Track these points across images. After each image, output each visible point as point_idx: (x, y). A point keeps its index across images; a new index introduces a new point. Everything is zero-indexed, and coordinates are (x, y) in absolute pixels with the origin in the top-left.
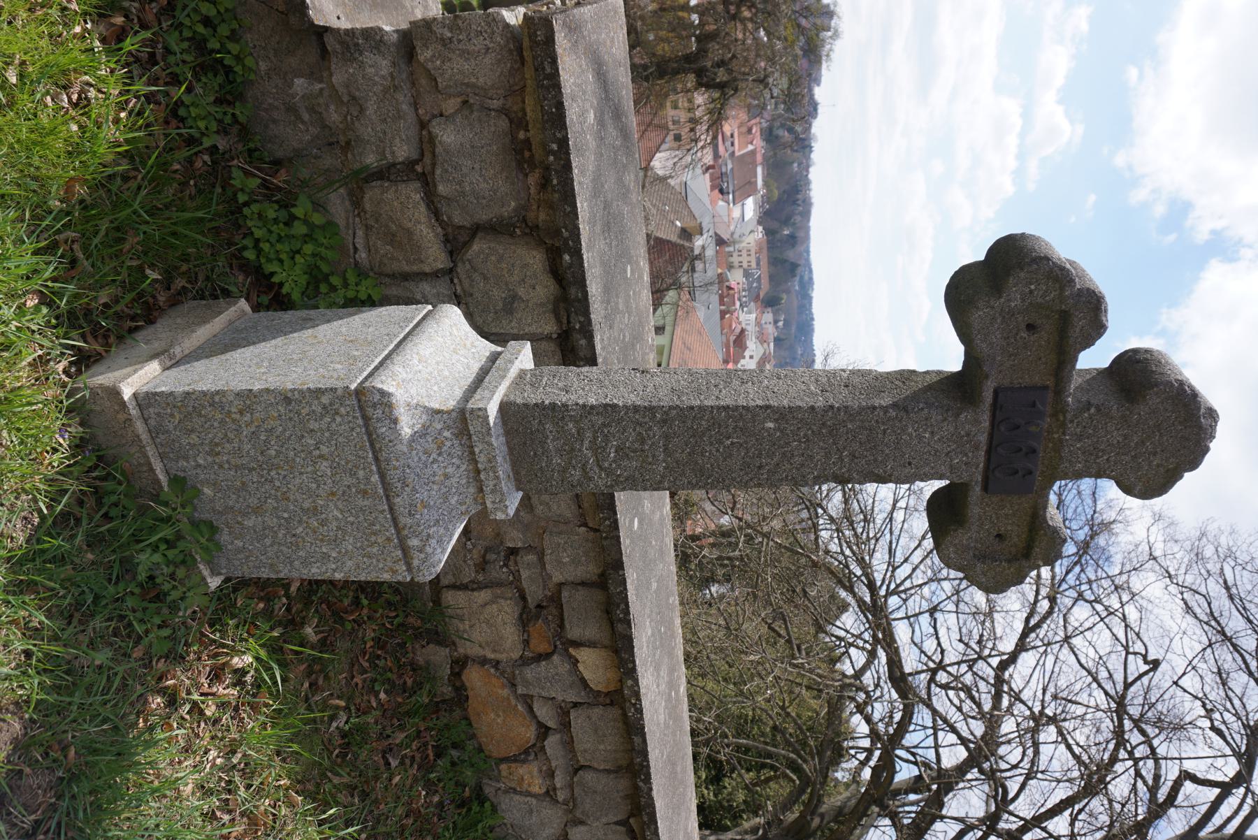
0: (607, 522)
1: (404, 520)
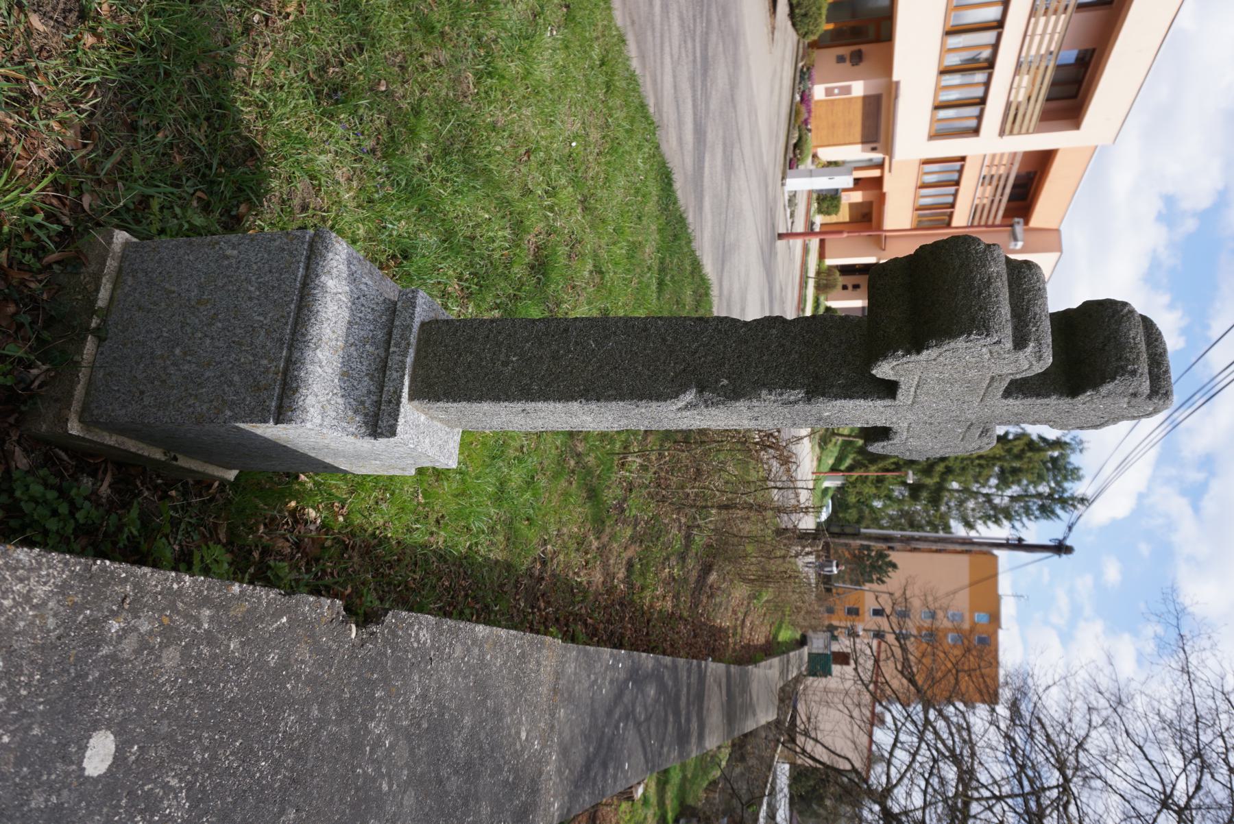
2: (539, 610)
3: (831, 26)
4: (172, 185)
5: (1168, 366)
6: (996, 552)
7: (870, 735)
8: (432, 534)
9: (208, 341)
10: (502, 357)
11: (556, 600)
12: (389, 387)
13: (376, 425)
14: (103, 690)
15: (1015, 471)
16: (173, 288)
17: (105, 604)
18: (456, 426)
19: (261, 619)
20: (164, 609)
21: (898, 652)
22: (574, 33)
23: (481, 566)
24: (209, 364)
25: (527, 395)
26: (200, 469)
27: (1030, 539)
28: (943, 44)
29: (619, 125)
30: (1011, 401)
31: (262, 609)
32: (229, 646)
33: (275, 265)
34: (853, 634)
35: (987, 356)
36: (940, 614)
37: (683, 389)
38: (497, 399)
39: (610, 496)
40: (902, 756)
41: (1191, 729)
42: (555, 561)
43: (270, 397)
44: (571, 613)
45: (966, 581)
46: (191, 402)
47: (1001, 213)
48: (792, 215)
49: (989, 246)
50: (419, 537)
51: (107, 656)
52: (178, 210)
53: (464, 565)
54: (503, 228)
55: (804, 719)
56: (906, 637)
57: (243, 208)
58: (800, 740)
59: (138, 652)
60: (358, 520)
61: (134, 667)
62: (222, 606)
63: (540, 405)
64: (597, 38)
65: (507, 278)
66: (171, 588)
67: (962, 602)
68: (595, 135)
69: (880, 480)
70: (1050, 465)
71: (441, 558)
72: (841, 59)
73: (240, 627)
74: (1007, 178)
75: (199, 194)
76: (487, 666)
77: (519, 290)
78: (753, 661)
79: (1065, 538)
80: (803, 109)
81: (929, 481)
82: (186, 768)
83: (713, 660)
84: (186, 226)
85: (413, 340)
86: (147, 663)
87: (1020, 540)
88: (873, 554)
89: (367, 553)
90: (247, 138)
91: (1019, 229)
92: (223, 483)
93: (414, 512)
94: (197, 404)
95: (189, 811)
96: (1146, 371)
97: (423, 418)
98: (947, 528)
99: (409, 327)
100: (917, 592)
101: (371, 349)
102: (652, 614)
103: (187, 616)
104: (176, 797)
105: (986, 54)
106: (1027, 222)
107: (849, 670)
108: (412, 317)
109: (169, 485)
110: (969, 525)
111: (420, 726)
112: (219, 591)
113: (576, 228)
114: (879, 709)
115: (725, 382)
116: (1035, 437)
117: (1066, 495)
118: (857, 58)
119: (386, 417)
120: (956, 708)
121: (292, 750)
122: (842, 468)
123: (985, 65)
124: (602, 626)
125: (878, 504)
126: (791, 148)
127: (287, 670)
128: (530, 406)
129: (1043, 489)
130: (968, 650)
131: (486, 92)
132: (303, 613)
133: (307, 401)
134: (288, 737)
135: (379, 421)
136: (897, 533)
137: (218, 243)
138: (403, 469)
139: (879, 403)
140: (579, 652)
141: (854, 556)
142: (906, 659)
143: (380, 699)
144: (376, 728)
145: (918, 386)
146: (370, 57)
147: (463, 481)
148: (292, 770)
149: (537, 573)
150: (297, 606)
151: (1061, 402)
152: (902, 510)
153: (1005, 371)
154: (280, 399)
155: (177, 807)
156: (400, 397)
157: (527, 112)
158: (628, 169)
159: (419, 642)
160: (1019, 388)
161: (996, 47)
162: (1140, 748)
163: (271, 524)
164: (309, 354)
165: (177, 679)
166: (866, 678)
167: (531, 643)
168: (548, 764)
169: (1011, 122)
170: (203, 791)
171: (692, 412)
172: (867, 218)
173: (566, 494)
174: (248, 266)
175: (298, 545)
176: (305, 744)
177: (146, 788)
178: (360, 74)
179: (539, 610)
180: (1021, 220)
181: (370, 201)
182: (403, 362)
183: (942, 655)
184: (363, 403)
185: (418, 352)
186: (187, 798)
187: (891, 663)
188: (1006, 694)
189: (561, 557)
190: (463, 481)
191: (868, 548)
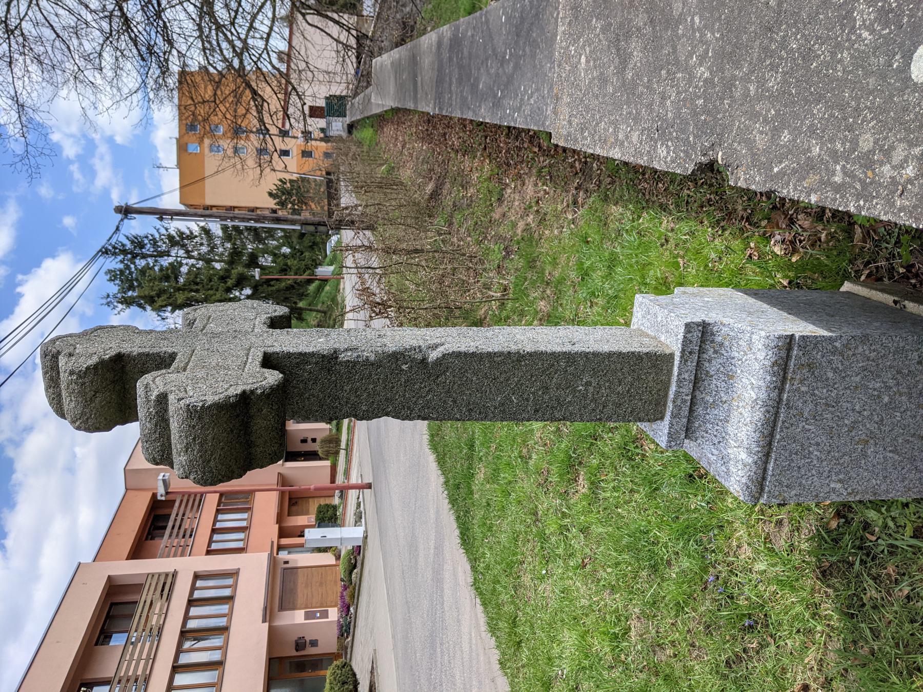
2: (580, 161)
3: (322, 673)
4: (897, 547)
5: (44, 378)
6: (182, 208)
7: (290, 46)
8: (672, 230)
9: (857, 408)
10: (591, 389)
11: (565, 169)
12: (692, 365)
13: (703, 333)
14: (919, 117)
15: (167, 278)
16: (891, 455)
17: (916, 190)
18: (634, 330)
19: (794, 171)
20: (871, 183)
21: (267, 119)
22: (544, 672)
23: (629, 201)
24: (856, 387)
25: (570, 358)
26: (874, 292)
27: (153, 219)
28: (225, 654)
29: (505, 588)
30: (170, 350)
31: (793, 180)
32: (821, 149)
33: (795, 474)
34: (307, 135)
35: (189, 388)
36: (230, 152)
37: (439, 362)
38: (596, 354)
39: (517, 262)
40: (262, 26)
41: (16, 56)
42: (565, 204)
43: (798, 358)
44: (553, 157)
45: (208, 182)
46: (873, 355)
47: (177, 504)
48: (359, 505)
49: (187, 477)
50: (684, 227)
51: (916, 145)
52: (891, 524)
53: (644, 202)
54: (605, 499)
55: (348, 60)
56: (259, 131)
57: (834, 524)
58: (353, 42)
59: (892, 148)
60: (737, 244)
61: (895, 135)
62: (826, 183)
63: (558, 349)
64: (523, 666)
65: (603, 454)
66: (865, 201)
67: (211, 162)
68: (526, 579)
69: (284, 270)
70: (135, 284)
71: (664, 208)
72: (314, 643)
73: (810, 166)
74: (170, 536)
75: (874, 538)
76: (611, 123)
77: (592, 444)
78: (396, 111)
79: (122, 220)
80: (347, 599)
81: (240, 269)
82: (856, 46)
83: (428, 114)
84: (883, 510)
85: (670, 405)
86: (885, 138)
87: (161, 219)
88: (290, 206)
89: (730, 213)
90: (828, 586)
91: (161, 490)
92: (856, 280)
93: (687, 250)
94: (867, 352)
95: (854, 9)
96: (62, 375)
97: (663, 339)
98: (225, 228)
99: (673, 416)
100: (251, 172)
101: (708, 398)
102: (482, 155)
103: (852, 175)
104: (864, 21)
105: (187, 645)
106: (154, 495)
107: (309, 102)
108: (671, 425)
109: (905, 277)
110: (206, 231)
111: (668, 72)
112: (827, 197)
113: (543, 498)
114: (283, 68)
115: (404, 367)
116: (149, 308)
117: (121, 257)
118: (300, 644)
119: (694, 340)
120: (215, 68)
121: (771, 56)
122: (317, 282)
123: (188, 635)
124: (526, 145)
125: (286, 250)
126: (359, 565)
127: (774, 126)
128: (567, 348)
129: (141, 263)
130: (206, 120)
131: (619, 620)
132: (761, 175)
133: (764, 354)
134: (774, 67)
135: (701, 337)
136: (267, 225)
137: (849, 494)
138: (685, 293)
139: (277, 349)
140: (543, 124)
141: (306, 204)
142: (260, 112)
143: (699, 97)
144: (703, 72)
145: (245, 364)
146: (720, 656)
147: (643, 277)
148: (772, 40)
149: (581, 194)
150: (765, 181)
151: (129, 350)
152: (264, 244)
153: (175, 376)
154: (788, 357)
155: (863, 13)
156: (681, 357)
157: (584, 602)
158: (498, 548)
159: (667, 146)
160: (163, 361)
161: (179, 651)
162: (58, 36)
163: (815, 242)
164: (763, 395)
165: (862, 123)
166: (294, 98)
167: (576, 140)
168: (563, 32)
169: (167, 584)
170: (843, 27)
171: (432, 342)
172: (292, 500)
173: (554, 263)
174: (820, 474)
175: (792, 222)
176: (761, 61)
177: (887, 31)
178: (728, 641)
179: (580, 161)
180: (159, 498)
181: (721, 527)
182: (679, 387)
183: (228, 116)
184: (716, 352)
185: (666, 395)
186: (855, 20)
187: (273, 109)
188: (172, 81)
189: (560, 208)
190: (643, 277)
191: (295, 212)
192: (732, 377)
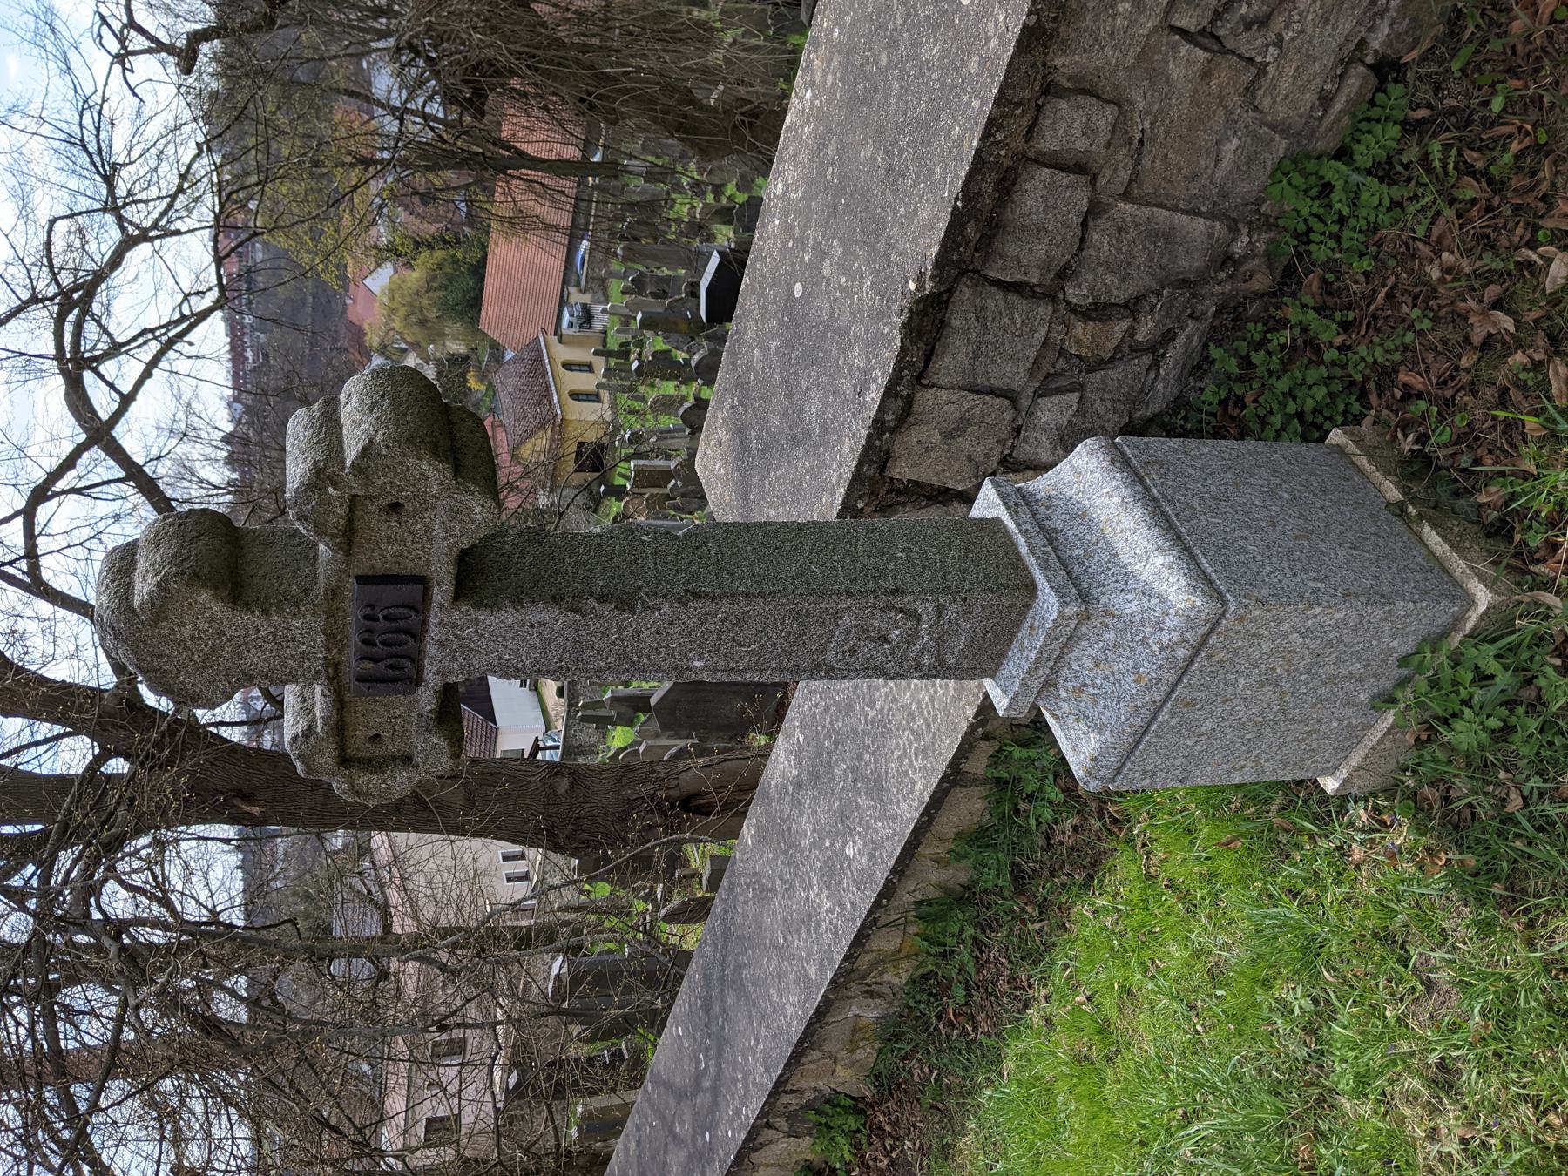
0: (999, 137)
1: (1169, 677)
85: (1030, 560)
99: (1045, 568)
164: (1127, 492)
184: (1048, 508)
192: (1085, 514)
